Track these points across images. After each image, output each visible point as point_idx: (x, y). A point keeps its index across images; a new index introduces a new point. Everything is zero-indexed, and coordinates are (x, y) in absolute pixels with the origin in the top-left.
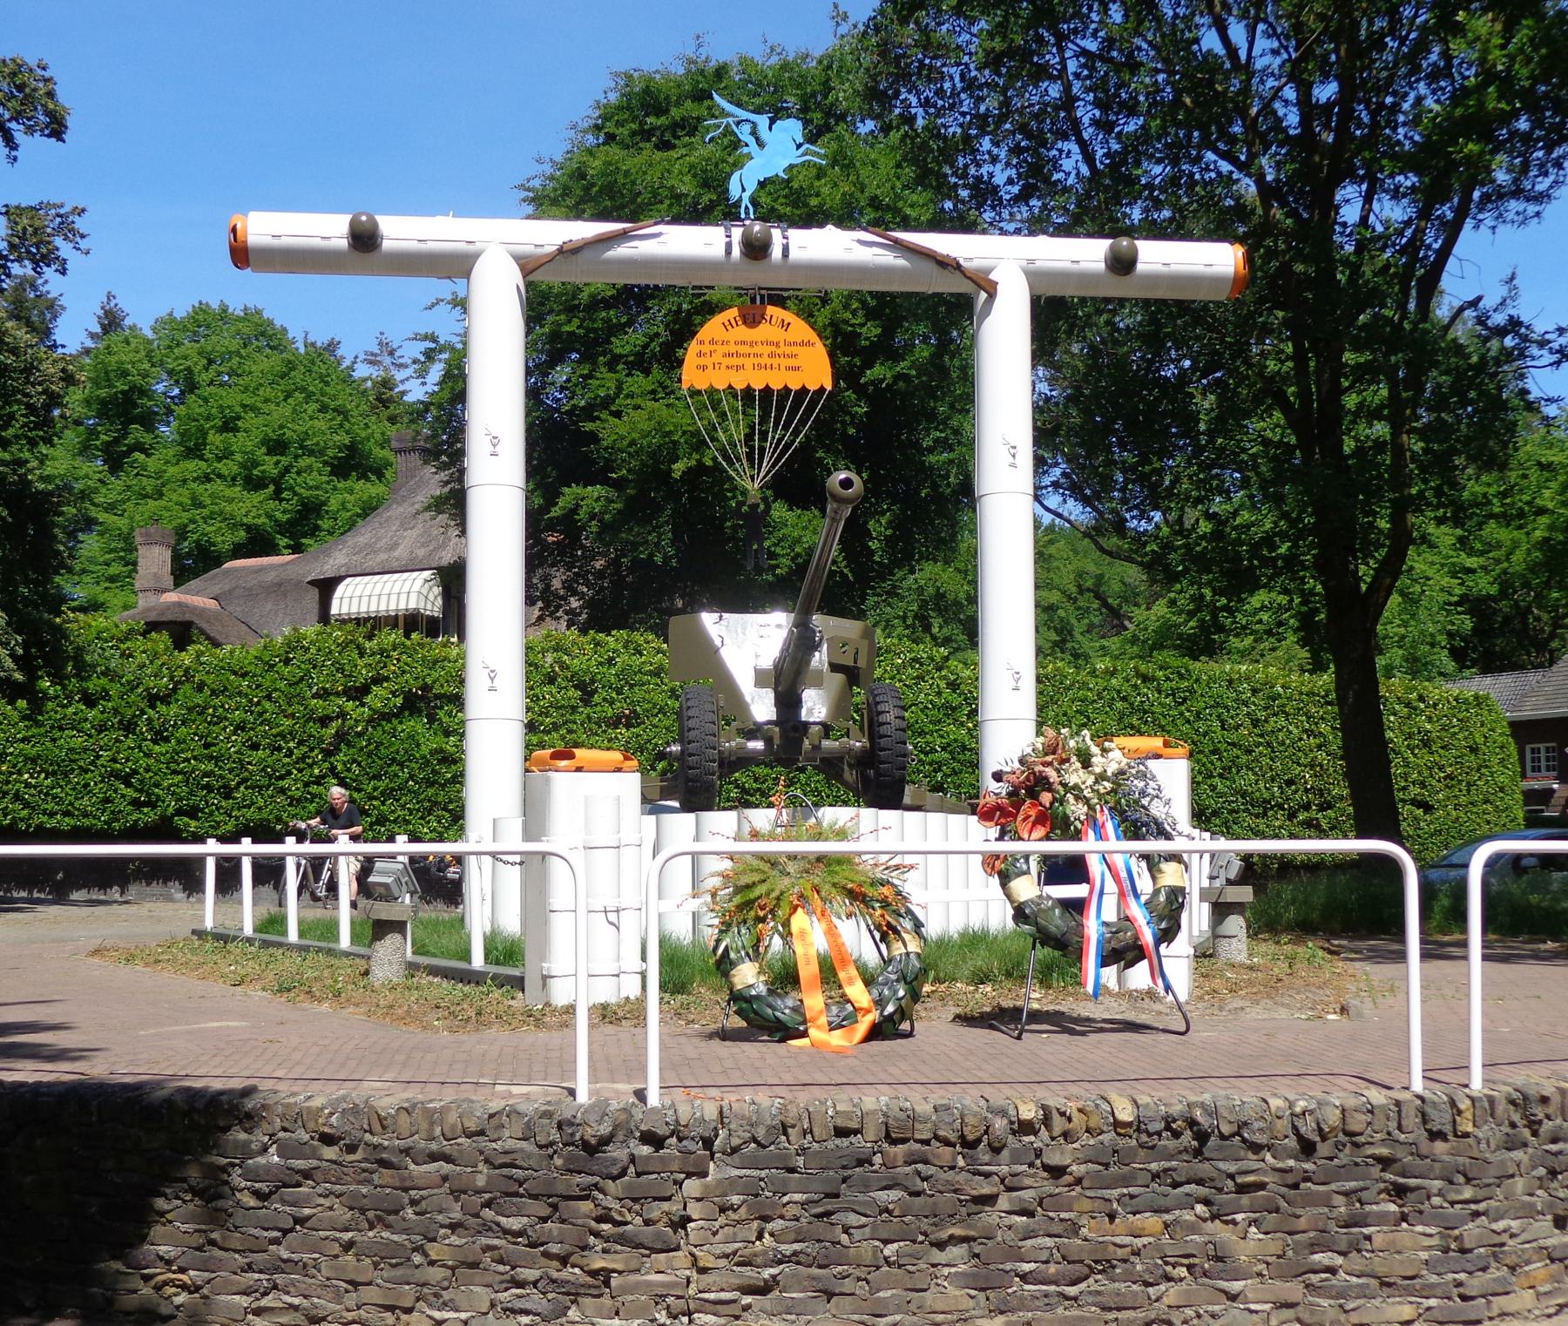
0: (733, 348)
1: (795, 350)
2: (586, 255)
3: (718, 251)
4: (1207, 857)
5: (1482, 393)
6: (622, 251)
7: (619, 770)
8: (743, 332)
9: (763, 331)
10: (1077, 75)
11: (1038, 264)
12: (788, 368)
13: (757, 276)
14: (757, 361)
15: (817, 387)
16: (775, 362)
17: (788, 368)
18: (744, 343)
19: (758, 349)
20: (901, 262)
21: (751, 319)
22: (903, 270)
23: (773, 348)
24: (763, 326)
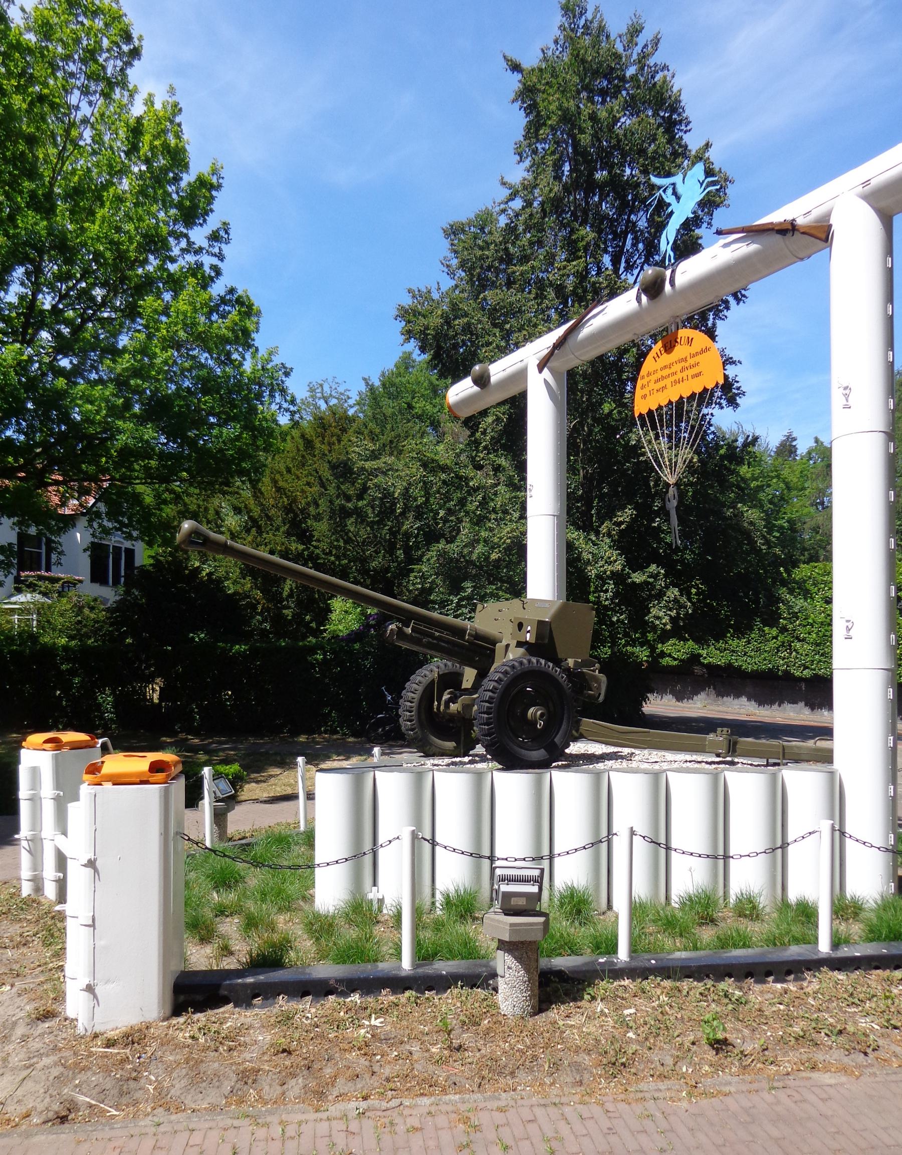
0: (658, 375)
1: (697, 359)
2: (570, 342)
3: (634, 305)
4: (534, 889)
5: (610, 368)
6: (586, 331)
7: (146, 782)
8: (666, 359)
9: (680, 351)
10: (119, 199)
11: (874, 182)
12: (694, 376)
13: (662, 315)
14: (672, 379)
15: (667, 402)
16: (684, 374)
17: (694, 376)
18: (665, 367)
19: (673, 369)
20: (754, 247)
21: (669, 347)
22: (756, 254)
23: (683, 364)
24: (678, 348)
